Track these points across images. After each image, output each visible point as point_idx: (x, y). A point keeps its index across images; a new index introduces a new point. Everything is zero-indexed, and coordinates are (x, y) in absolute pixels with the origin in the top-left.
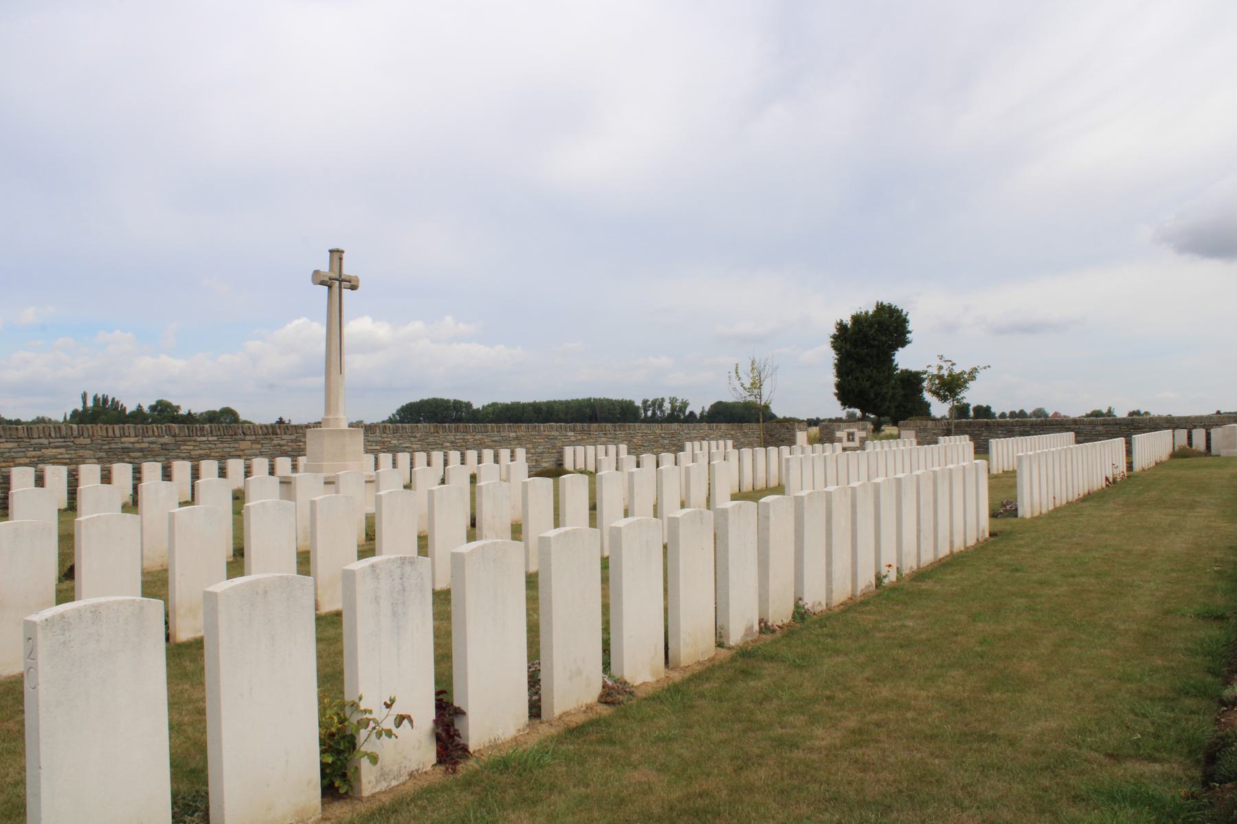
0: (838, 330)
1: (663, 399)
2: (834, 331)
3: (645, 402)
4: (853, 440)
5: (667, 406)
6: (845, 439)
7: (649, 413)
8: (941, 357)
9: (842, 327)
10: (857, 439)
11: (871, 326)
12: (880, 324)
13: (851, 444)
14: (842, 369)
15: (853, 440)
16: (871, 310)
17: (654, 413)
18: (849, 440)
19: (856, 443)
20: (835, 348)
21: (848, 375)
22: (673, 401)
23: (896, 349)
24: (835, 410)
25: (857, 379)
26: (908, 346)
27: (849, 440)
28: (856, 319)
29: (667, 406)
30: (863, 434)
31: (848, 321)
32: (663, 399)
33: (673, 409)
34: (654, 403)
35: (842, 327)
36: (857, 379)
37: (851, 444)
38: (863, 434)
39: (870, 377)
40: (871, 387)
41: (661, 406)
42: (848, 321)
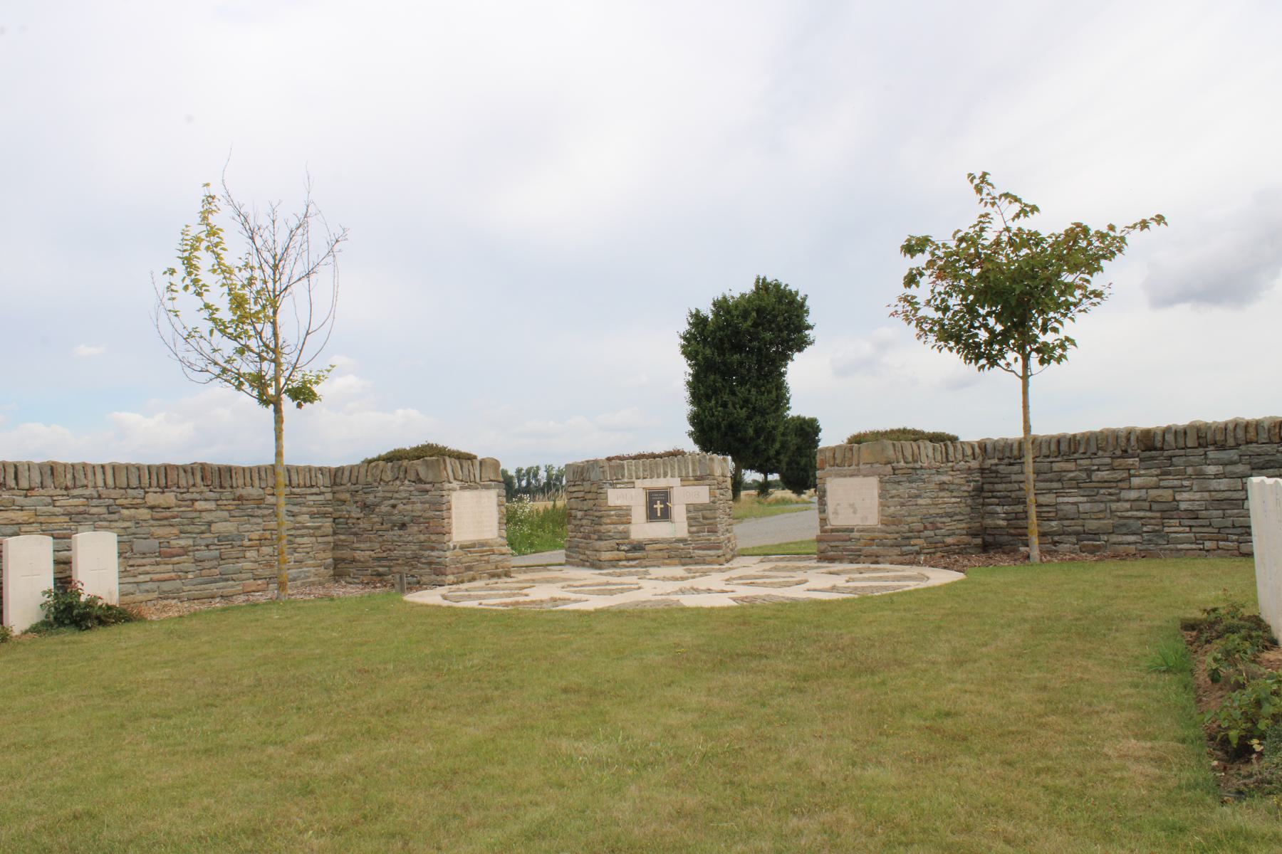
0: (694, 325)
1: (538, 468)
2: (684, 327)
3: (519, 471)
4: (666, 515)
5: (543, 475)
6: (639, 513)
7: (524, 483)
8: (981, 183)
9: (698, 321)
10: (679, 512)
11: (745, 314)
12: (760, 311)
13: (661, 530)
14: (701, 390)
15: (666, 515)
16: (748, 288)
17: (529, 483)
18: (652, 516)
19: (677, 528)
20: (689, 353)
21: (709, 399)
22: (549, 469)
23: (785, 358)
24: (691, 447)
25: (725, 405)
26: (808, 349)
27: (652, 516)
28: (721, 306)
29: (543, 475)
30: (701, 494)
31: (707, 311)
32: (538, 468)
33: (549, 477)
34: (528, 472)
35: (698, 321)
36: (725, 405)
37: (661, 530)
38: (701, 494)
39: (746, 401)
40: (749, 418)
41: (536, 475)
42: (707, 311)
